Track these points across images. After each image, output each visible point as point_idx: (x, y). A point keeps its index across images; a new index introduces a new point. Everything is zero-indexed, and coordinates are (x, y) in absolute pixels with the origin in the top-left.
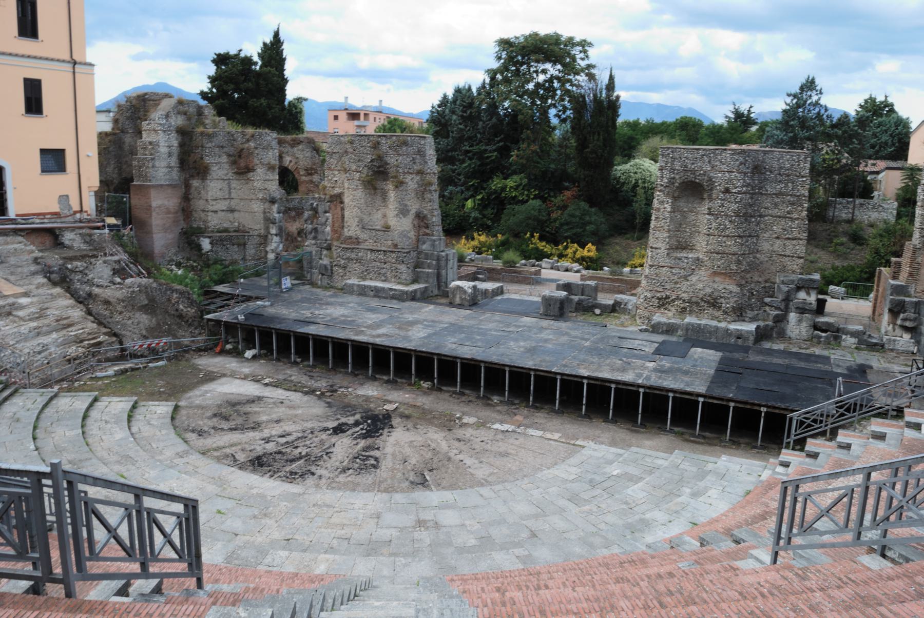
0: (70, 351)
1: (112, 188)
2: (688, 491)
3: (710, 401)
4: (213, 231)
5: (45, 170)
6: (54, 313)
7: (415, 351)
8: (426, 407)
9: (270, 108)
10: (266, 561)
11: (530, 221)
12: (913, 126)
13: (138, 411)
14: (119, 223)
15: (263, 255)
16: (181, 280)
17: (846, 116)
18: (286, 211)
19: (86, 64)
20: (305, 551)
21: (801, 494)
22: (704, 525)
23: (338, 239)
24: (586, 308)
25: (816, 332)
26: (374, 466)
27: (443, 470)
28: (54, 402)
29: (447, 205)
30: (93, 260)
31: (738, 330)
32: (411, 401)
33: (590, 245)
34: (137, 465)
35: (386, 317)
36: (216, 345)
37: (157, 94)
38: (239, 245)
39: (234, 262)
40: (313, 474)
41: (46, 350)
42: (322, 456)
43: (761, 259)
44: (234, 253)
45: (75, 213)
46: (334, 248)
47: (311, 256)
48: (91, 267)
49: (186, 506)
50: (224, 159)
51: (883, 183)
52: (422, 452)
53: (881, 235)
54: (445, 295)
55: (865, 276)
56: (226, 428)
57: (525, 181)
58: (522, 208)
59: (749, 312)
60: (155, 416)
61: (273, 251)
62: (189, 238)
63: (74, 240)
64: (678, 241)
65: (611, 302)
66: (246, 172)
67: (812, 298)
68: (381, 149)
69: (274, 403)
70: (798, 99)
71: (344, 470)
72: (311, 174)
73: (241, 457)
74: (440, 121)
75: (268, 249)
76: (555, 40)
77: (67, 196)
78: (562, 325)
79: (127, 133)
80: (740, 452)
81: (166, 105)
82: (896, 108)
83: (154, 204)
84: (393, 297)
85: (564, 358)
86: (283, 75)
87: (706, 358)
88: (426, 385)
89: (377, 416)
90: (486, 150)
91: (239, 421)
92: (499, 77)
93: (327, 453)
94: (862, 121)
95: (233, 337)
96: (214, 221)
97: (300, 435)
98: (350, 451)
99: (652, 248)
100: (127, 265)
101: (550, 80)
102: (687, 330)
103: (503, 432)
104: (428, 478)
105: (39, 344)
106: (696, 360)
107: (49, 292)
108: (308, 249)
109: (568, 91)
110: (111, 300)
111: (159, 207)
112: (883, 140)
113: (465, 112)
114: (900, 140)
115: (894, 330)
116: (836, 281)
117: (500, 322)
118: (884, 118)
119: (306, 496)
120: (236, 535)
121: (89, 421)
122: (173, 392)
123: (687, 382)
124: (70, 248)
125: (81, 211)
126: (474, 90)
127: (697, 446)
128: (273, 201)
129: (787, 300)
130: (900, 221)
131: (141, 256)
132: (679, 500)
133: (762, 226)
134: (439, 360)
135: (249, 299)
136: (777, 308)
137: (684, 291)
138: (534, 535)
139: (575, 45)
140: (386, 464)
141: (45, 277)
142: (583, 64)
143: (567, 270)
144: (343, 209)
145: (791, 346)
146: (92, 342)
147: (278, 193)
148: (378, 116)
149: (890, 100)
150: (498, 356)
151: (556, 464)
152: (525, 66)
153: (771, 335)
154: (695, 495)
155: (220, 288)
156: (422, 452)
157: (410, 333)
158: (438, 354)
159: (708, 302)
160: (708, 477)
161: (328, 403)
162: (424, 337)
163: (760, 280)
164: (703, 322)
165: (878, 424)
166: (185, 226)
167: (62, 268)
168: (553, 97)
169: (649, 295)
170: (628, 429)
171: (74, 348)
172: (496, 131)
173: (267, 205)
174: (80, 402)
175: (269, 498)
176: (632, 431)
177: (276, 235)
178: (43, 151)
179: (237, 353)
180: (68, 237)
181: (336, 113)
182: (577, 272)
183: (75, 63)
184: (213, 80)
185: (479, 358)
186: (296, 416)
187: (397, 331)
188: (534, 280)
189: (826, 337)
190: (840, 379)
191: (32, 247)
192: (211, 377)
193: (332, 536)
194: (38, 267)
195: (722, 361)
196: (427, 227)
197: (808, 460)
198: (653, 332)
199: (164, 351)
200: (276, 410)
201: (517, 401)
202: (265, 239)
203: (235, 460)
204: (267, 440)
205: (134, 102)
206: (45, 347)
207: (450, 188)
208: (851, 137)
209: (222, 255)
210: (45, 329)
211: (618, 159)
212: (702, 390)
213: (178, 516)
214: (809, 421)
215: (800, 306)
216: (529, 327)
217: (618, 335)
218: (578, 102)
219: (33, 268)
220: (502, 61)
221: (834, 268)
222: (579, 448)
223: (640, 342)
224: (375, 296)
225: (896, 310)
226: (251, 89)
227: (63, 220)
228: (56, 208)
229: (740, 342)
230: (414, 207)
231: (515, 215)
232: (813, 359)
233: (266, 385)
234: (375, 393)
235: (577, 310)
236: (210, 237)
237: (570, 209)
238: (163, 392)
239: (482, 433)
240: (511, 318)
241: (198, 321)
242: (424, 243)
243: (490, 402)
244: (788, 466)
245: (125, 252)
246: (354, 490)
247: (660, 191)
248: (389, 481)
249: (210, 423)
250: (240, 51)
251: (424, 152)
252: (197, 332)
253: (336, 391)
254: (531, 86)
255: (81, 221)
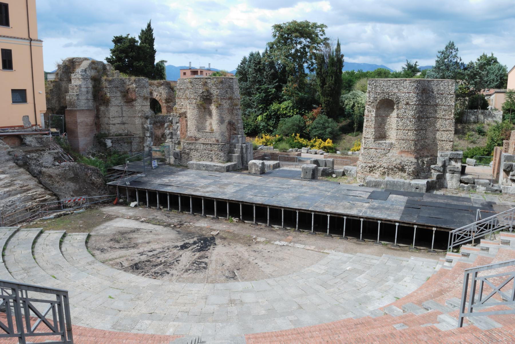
0: (28, 204)
1: (55, 112)
2: (392, 278)
3: (403, 225)
4: (113, 136)
5: (14, 102)
6: (19, 182)
7: (229, 200)
8: (235, 232)
9: (146, 66)
10: (137, 327)
11: (294, 127)
12: (508, 70)
13: (66, 239)
14: (58, 131)
15: (142, 148)
16: (93, 163)
17: (472, 63)
18: (155, 123)
19: (37, 40)
20: (161, 320)
21: (479, 278)
22: (404, 299)
23: (184, 138)
24: (327, 174)
25: (462, 184)
26: (204, 268)
27: (246, 269)
28: (17, 234)
29: (247, 119)
30: (42, 152)
31: (416, 184)
32: (227, 230)
33: (329, 139)
34: (63, 270)
35: (212, 181)
36: (114, 200)
37: (80, 58)
38: (128, 143)
39: (125, 153)
40: (168, 273)
41: (14, 204)
42: (174, 263)
43: (428, 143)
44: (125, 148)
45: (33, 126)
46: (182, 143)
47: (169, 148)
48: (41, 156)
49: (58, 296)
50: (119, 94)
51: (494, 101)
52: (233, 259)
53: (494, 130)
54: (247, 169)
55: (486, 153)
56: (117, 247)
57: (291, 105)
58: (290, 120)
59: (422, 173)
60: (76, 241)
61: (147, 146)
62: (99, 139)
63: (32, 141)
64: (380, 134)
65: (342, 170)
66: (131, 102)
67: (459, 165)
68: (209, 89)
69: (147, 232)
70: (445, 54)
71: (187, 271)
72: (169, 102)
73: (126, 264)
74: (242, 73)
75: (145, 145)
76: (307, 25)
77: (28, 116)
78: (314, 183)
79: (64, 80)
80: (421, 254)
81: (85, 65)
82: (498, 60)
83: (79, 121)
84: (216, 170)
85: (316, 202)
86: (153, 48)
87: (398, 202)
88: (235, 220)
89: (207, 238)
90: (268, 88)
91: (126, 243)
92: (275, 46)
93: (177, 261)
94: (482, 67)
95: (124, 195)
96: (113, 130)
97: (161, 250)
98: (191, 259)
99: (365, 138)
100: (62, 155)
101: (304, 48)
102: (387, 184)
103: (281, 246)
104: (236, 274)
105: (10, 201)
106: (393, 202)
107: (16, 171)
108: (167, 144)
109: (314, 53)
110: (52, 175)
111: (82, 122)
112: (492, 78)
113: (256, 66)
114: (501, 78)
115: (507, 182)
116: (469, 156)
117: (278, 182)
118: (492, 66)
119: (163, 287)
120: (120, 311)
121: (37, 245)
122: (88, 227)
123: (388, 214)
124: (30, 146)
125: (36, 125)
126: (261, 54)
127: (396, 251)
128: (147, 118)
129: (444, 166)
130: (505, 121)
131: (72, 150)
132: (387, 284)
133: (429, 124)
134: (242, 205)
135: (133, 173)
136: (439, 171)
137: (384, 162)
138: (300, 307)
139: (317, 27)
140: (212, 266)
141: (15, 162)
142: (322, 38)
143: (316, 153)
144: (186, 121)
145: (447, 193)
146: (41, 199)
147: (149, 113)
148: (208, 72)
149: (495, 56)
150: (277, 202)
151: (312, 264)
152: (289, 40)
153: (436, 186)
154: (397, 280)
155: (117, 168)
156: (233, 259)
157: (226, 190)
158: (242, 202)
159: (398, 168)
160: (404, 270)
161: (178, 231)
162: (234, 192)
163: (428, 155)
164: (396, 180)
165: (505, 235)
166: (97, 133)
167: (25, 157)
168: (305, 57)
169: (364, 165)
170: (355, 243)
171: (30, 203)
172: (274, 76)
173: (144, 120)
174: (33, 233)
175: (141, 288)
176: (357, 244)
177: (149, 137)
178: (13, 91)
179: (126, 204)
180: (28, 140)
181: (185, 71)
182: (322, 154)
183: (31, 40)
184: (113, 52)
185: (266, 203)
186: (159, 239)
187: (218, 189)
188: (297, 160)
189: (468, 187)
190: (479, 210)
191: (7, 146)
192: (110, 218)
193: (178, 310)
194: (11, 157)
195: (408, 202)
196: (235, 130)
197: (463, 258)
198: (367, 186)
199: (83, 204)
200: (147, 236)
201: (288, 228)
202: (143, 139)
203: (122, 266)
204: (142, 254)
205: (67, 63)
206: (13, 202)
207: (249, 109)
208: (475, 75)
209: (118, 149)
210: (13, 192)
211: (343, 91)
212: (398, 218)
213: (52, 303)
214: (462, 235)
215: (452, 169)
216: (295, 185)
217: (347, 188)
218: (321, 59)
219: (7, 157)
220: (277, 37)
221: (469, 149)
222: (326, 254)
223: (360, 192)
224: (206, 170)
225: (508, 170)
226: (136, 56)
227: (26, 130)
228: (21, 123)
229: (418, 191)
230: (227, 118)
231: (285, 124)
232: (461, 199)
233: (142, 222)
234: (206, 225)
235: (322, 175)
236: (111, 139)
237: (317, 119)
238: (82, 227)
239: (269, 247)
240: (284, 180)
241: (104, 187)
242: (233, 139)
243: (273, 229)
244: (451, 262)
245: (62, 147)
246: (192, 282)
247: (369, 105)
248: (213, 277)
249: (109, 245)
250: (128, 35)
251: (232, 87)
252: (102, 192)
253: (183, 224)
254: (293, 51)
255: (36, 131)
